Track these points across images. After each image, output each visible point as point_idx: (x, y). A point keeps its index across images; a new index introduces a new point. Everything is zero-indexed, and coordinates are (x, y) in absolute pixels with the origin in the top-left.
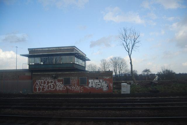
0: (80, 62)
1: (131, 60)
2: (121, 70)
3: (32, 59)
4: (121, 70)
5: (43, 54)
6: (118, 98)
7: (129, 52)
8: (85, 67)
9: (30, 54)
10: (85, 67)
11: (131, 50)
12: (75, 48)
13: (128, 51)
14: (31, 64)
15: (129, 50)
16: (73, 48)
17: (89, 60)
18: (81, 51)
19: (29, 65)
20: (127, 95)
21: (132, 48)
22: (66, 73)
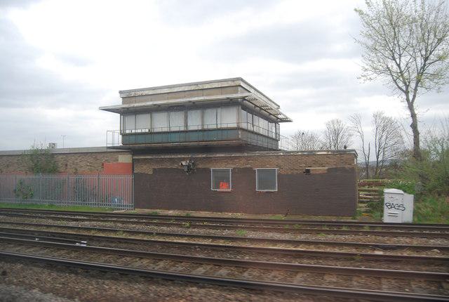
0: (262, 126)
1: (413, 116)
2: (381, 150)
3: (130, 120)
4: (381, 150)
5: (155, 103)
6: (115, 219)
7: (407, 93)
8: (277, 141)
9: (124, 106)
10: (277, 141)
11: (413, 85)
12: (242, 84)
13: (404, 88)
14: (127, 132)
15: (407, 88)
16: (237, 83)
17: (286, 120)
18: (264, 96)
19: (124, 135)
20: (394, 229)
21: (418, 81)
22: (218, 155)
